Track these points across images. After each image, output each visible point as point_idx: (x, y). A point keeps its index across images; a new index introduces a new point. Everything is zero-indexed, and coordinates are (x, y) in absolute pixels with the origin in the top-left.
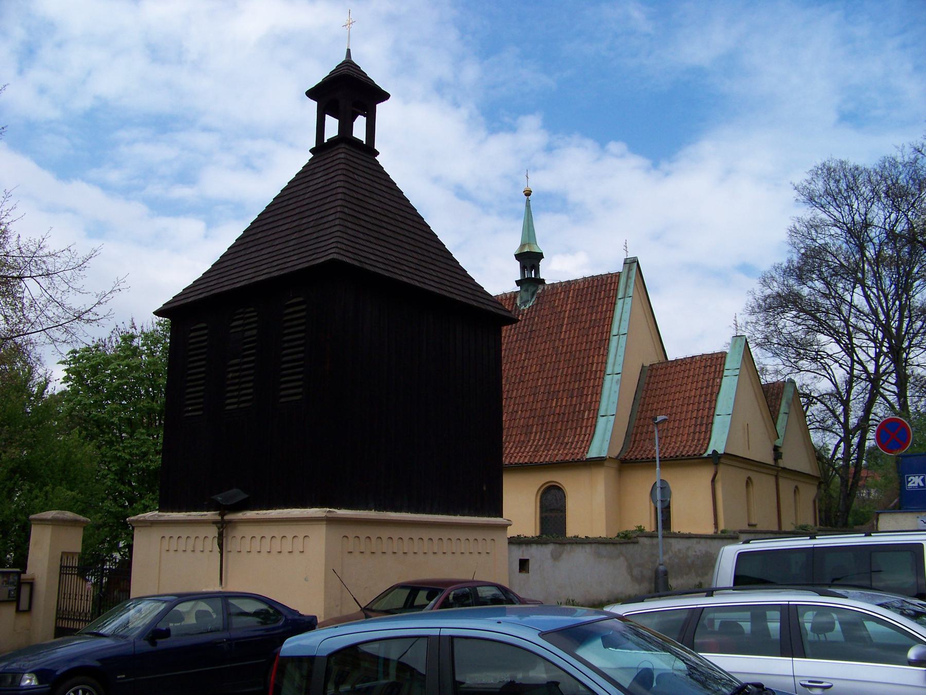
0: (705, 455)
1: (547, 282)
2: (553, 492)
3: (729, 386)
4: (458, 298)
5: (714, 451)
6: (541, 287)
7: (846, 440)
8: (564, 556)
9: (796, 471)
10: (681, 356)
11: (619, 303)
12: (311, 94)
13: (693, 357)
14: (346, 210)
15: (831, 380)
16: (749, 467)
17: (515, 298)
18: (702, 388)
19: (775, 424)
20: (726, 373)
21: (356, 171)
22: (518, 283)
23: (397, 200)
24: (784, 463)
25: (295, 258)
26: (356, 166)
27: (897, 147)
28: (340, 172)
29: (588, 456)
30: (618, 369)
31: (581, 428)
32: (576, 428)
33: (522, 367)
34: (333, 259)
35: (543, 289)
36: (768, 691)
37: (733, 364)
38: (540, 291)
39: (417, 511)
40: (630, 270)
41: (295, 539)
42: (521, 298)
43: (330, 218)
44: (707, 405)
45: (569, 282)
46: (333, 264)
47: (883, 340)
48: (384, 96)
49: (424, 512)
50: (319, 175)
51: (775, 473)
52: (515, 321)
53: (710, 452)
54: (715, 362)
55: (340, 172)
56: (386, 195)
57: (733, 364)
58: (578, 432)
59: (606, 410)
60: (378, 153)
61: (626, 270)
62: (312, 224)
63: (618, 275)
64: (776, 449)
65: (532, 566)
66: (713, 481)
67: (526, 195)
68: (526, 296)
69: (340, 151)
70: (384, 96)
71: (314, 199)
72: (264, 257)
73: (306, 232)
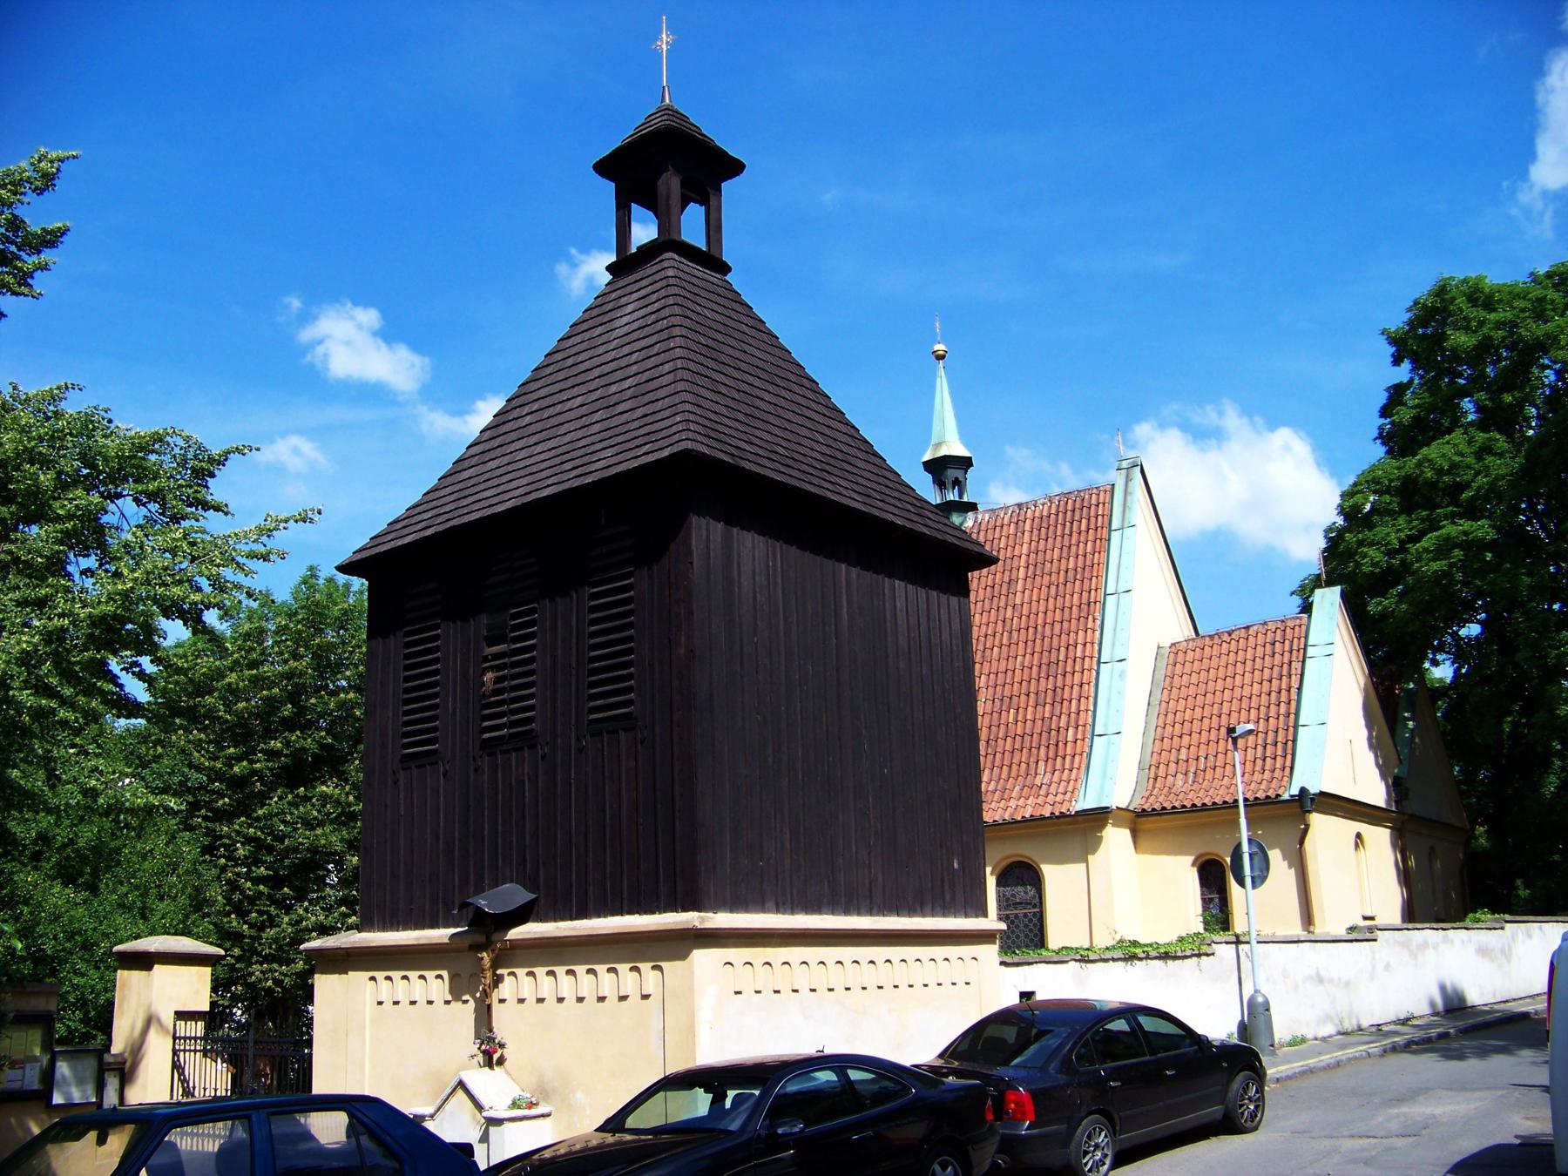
0: (1286, 796)
4: (899, 522)
5: (1303, 790)
9: (1430, 820)
12: (603, 168)
14: (692, 366)
21: (698, 300)
23: (770, 349)
25: (609, 453)
26: (696, 290)
28: (671, 301)
34: (686, 450)
36: (101, 1037)
39: (847, 911)
43: (665, 380)
46: (684, 461)
48: (735, 168)
49: (859, 912)
50: (630, 308)
52: (995, 561)
53: (1295, 791)
55: (671, 301)
56: (751, 341)
59: (1105, 725)
60: (729, 269)
62: (629, 393)
69: (666, 264)
70: (735, 168)
71: (626, 350)
72: (542, 457)
73: (620, 408)
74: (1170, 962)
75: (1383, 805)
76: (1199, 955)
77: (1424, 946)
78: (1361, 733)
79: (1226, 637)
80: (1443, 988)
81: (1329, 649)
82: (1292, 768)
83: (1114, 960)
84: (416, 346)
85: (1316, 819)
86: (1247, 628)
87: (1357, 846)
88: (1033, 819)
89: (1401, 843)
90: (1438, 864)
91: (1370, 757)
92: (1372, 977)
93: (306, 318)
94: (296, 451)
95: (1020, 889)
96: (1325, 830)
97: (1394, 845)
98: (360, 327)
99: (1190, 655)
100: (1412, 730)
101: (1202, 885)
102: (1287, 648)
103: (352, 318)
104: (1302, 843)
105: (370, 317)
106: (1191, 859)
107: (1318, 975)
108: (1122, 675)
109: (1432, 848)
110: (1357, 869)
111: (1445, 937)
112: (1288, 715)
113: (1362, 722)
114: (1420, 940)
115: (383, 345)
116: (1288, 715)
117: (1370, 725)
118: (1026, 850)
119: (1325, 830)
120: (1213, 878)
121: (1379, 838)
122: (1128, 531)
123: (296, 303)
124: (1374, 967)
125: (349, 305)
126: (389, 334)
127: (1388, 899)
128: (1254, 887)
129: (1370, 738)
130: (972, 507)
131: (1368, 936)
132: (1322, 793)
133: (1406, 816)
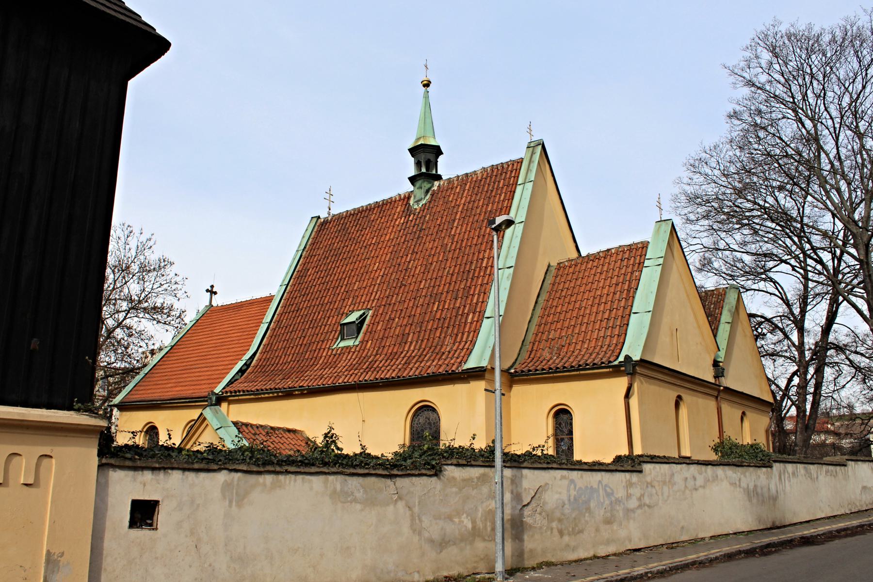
0: (616, 363)
1: (444, 178)
2: (426, 413)
3: (649, 277)
5: (627, 357)
6: (436, 183)
7: (801, 372)
8: (256, 495)
9: (742, 393)
10: (594, 250)
11: (519, 189)
13: (608, 250)
15: (782, 299)
16: (679, 382)
17: (409, 198)
18: (617, 285)
19: (715, 336)
20: (647, 263)
22: (413, 180)
24: (728, 382)
27: (865, 10)
29: (466, 367)
30: (512, 262)
31: (463, 334)
32: (457, 335)
33: (406, 270)
35: (439, 186)
37: (656, 252)
38: (435, 188)
40: (533, 153)
41: (46, 461)
42: (415, 197)
44: (622, 303)
45: (467, 174)
47: (845, 244)
51: (716, 393)
53: (621, 358)
54: (636, 253)
57: (656, 252)
58: (458, 339)
61: (529, 155)
63: (520, 162)
64: (716, 364)
65: (162, 516)
66: (627, 396)
67: (424, 86)
68: (419, 194)
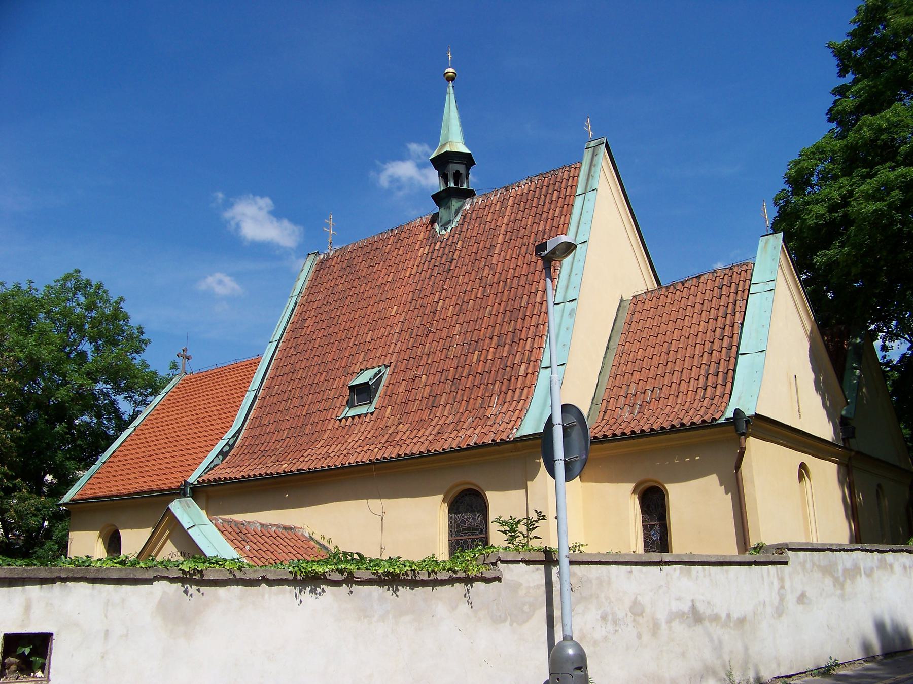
0: (722, 420)
5: (737, 412)
9: (878, 459)
53: (729, 414)
74: (404, 591)
75: (830, 440)
76: (469, 580)
77: (854, 572)
78: (807, 376)
79: (679, 287)
80: (880, 627)
81: (771, 285)
82: (731, 395)
83: (271, 583)
84: (294, 220)
85: (753, 445)
86: (699, 277)
87: (801, 478)
88: (477, 446)
89: (848, 477)
90: (886, 502)
91: (818, 399)
92: (780, 611)
93: (228, 205)
94: (220, 282)
95: (469, 515)
96: (760, 455)
97: (841, 482)
98: (260, 208)
99: (648, 304)
100: (859, 377)
101: (643, 512)
102: (733, 289)
103: (256, 203)
104: (738, 467)
105: (265, 202)
106: (631, 486)
107: (694, 608)
108: (572, 313)
109: (879, 486)
110: (798, 497)
111: (880, 561)
112: (730, 348)
113: (809, 366)
114: (849, 565)
115: (275, 219)
116: (730, 348)
117: (817, 368)
118: (473, 478)
119: (760, 455)
120: (653, 504)
121: (826, 472)
122: (590, 195)
123: (220, 195)
124: (782, 599)
125: (251, 196)
126: (278, 213)
127: (839, 530)
128: (568, 478)
129: (817, 382)
130: (470, 194)
131: (776, 557)
132: (757, 416)
133: (851, 452)
